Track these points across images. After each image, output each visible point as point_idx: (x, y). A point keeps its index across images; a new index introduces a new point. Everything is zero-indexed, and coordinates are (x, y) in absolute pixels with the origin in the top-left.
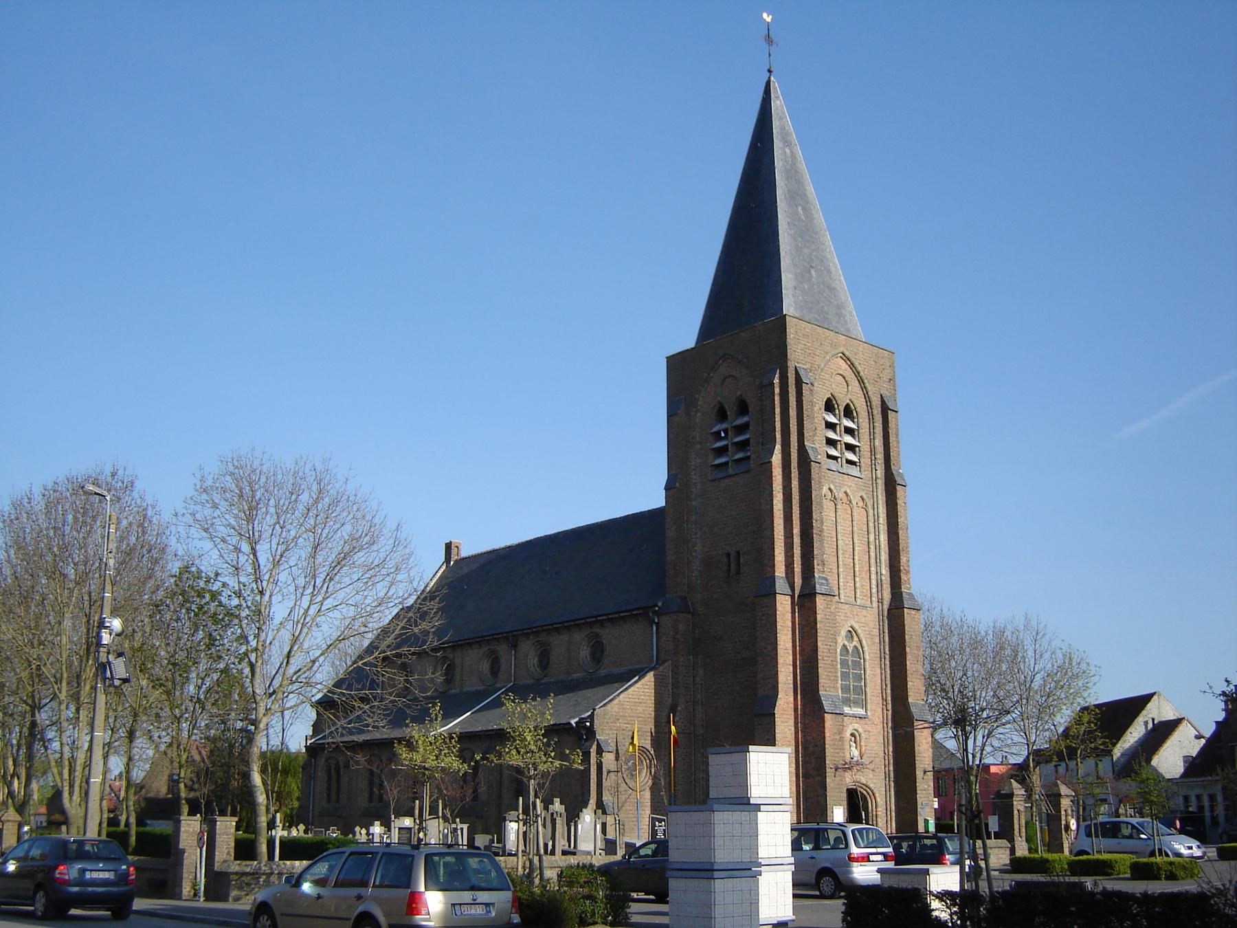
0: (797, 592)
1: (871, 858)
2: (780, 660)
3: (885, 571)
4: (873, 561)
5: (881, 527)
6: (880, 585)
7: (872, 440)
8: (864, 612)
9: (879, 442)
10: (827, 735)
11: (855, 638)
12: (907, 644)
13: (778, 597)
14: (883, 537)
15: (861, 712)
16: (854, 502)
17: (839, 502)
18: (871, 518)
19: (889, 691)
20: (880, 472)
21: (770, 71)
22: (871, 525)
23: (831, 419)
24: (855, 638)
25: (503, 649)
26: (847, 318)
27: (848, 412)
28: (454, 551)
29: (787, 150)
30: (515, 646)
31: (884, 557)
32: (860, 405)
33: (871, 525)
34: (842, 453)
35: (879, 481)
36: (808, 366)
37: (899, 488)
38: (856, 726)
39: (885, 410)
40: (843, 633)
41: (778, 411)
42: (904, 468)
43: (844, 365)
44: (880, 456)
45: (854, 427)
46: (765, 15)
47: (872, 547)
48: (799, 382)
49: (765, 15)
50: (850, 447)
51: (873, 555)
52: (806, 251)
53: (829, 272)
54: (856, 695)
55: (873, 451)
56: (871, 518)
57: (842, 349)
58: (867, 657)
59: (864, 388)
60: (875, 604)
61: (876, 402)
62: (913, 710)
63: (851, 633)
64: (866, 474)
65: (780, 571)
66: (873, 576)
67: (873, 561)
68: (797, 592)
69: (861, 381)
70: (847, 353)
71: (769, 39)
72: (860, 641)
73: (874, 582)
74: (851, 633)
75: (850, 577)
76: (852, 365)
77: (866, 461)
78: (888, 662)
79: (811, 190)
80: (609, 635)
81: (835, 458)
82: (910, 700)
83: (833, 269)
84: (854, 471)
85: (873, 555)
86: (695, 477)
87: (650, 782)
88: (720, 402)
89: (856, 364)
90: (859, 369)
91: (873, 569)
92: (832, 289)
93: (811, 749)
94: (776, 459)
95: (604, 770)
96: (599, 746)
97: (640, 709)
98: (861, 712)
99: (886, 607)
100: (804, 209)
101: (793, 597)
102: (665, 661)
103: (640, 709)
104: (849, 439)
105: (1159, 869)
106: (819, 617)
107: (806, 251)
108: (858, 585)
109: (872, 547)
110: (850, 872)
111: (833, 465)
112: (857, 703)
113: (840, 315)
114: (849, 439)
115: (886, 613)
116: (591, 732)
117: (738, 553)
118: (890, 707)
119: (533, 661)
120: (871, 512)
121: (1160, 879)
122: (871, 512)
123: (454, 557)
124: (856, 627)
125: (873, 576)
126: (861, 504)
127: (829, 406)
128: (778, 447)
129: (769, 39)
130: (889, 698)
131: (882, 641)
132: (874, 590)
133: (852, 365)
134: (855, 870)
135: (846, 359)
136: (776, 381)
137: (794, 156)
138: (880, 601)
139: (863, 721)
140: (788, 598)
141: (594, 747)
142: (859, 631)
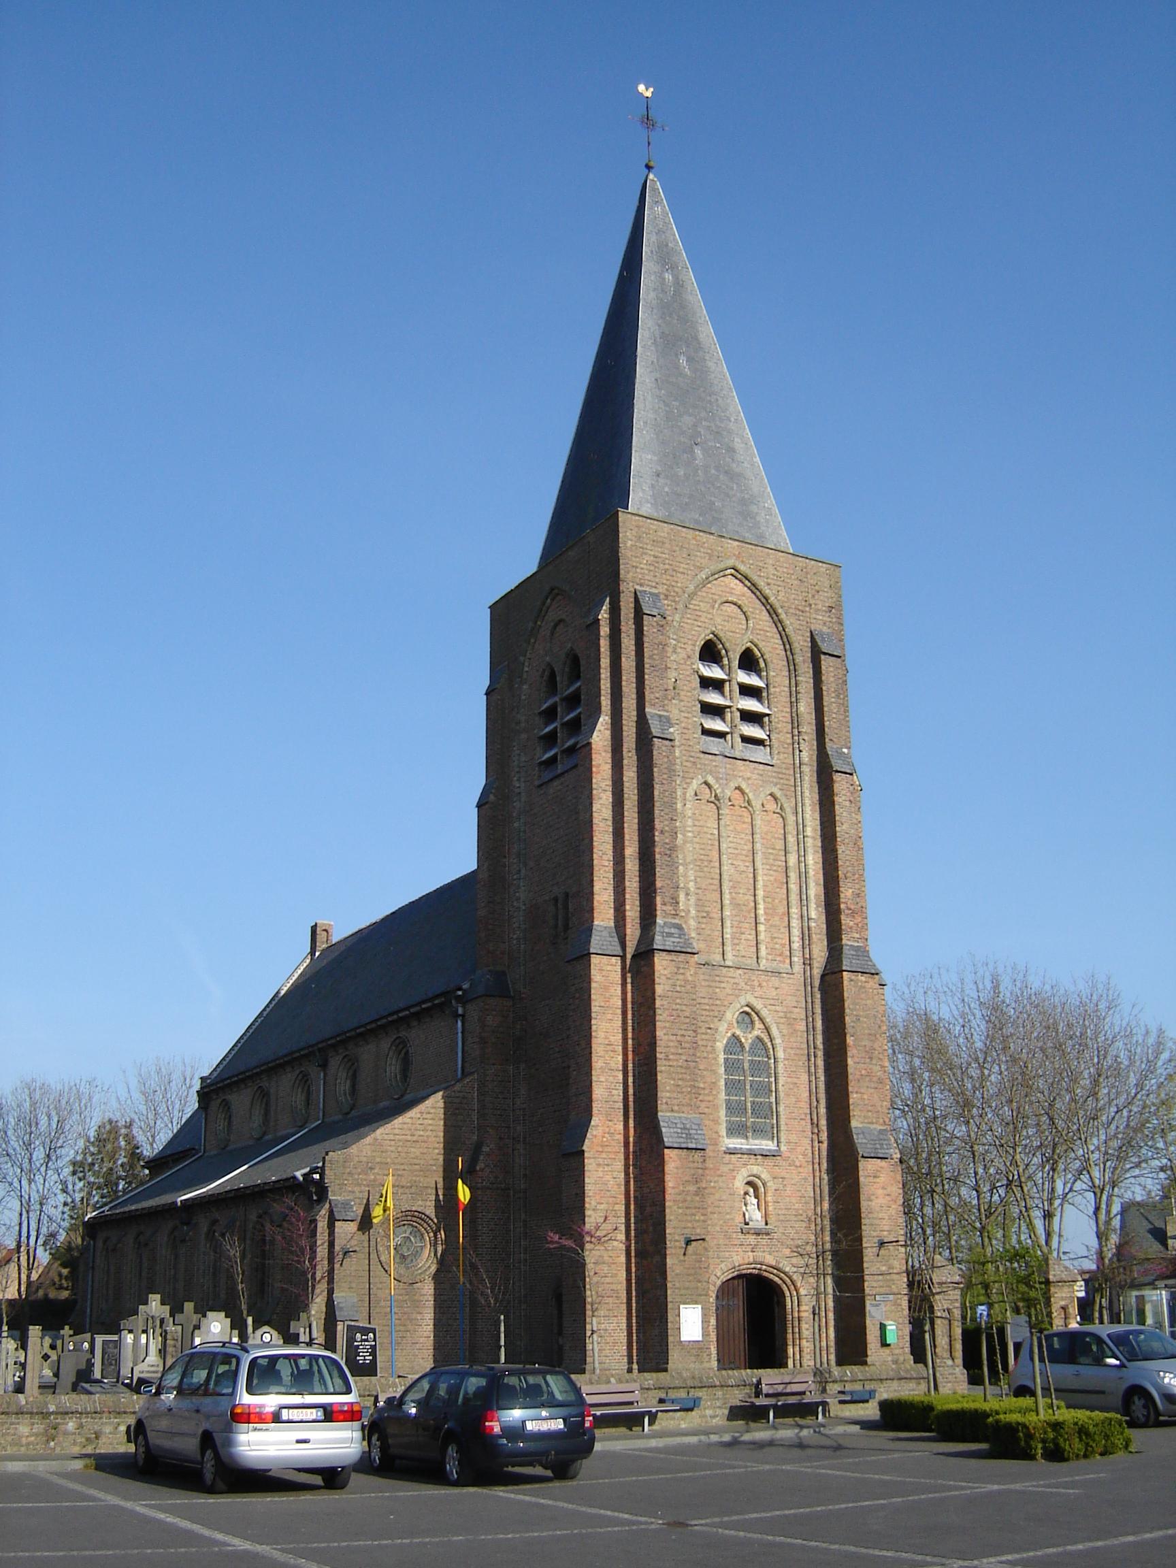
0: (629, 956)
1: (285, 1414)
2: (597, 1063)
3: (816, 913)
4: (794, 898)
5: (809, 842)
6: (806, 936)
7: (794, 703)
8: (775, 981)
9: (806, 707)
10: (670, 1183)
11: (758, 1025)
12: (849, 1030)
13: (595, 960)
14: (814, 860)
15: (768, 1145)
16: (757, 804)
17: (725, 804)
18: (791, 828)
19: (823, 1110)
20: (808, 754)
21: (649, 167)
22: (791, 839)
23: (715, 672)
24: (758, 1025)
25: (313, 1071)
26: (761, 518)
27: (749, 661)
28: (321, 936)
29: (668, 277)
30: (324, 1066)
31: (815, 890)
32: (770, 648)
33: (791, 839)
34: (734, 726)
35: (806, 769)
36: (661, 589)
37: (837, 777)
38: (756, 1169)
39: (816, 654)
40: (731, 1015)
41: (605, 662)
42: (858, 746)
43: (738, 589)
44: (808, 728)
45: (761, 684)
46: (641, 88)
47: (793, 876)
48: (639, 614)
49: (641, 88)
50: (749, 717)
51: (794, 887)
52: (687, 420)
53: (731, 450)
54: (753, 1114)
55: (795, 721)
56: (791, 828)
57: (731, 563)
58: (780, 1054)
59: (778, 622)
60: (798, 968)
61: (801, 644)
62: (858, 1140)
63: (749, 1016)
64: (781, 758)
65: (603, 917)
66: (795, 923)
67: (794, 898)
68: (630, 951)
69: (772, 612)
70: (742, 568)
71: (648, 121)
72: (767, 1029)
73: (796, 932)
74: (749, 1016)
75: (748, 926)
76: (754, 588)
77: (782, 737)
78: (820, 1063)
79: (707, 332)
80: (416, 1036)
81: (721, 735)
82: (854, 1123)
83: (738, 444)
84: (760, 754)
85: (794, 887)
86: (518, 784)
87: (434, 1268)
88: (549, 664)
89: (761, 584)
90: (767, 591)
91: (794, 911)
92: (733, 476)
93: (648, 1209)
94: (600, 737)
95: (337, 1248)
96: (331, 1212)
97: (415, 1151)
98: (768, 1145)
99: (817, 972)
100: (690, 360)
101: (623, 958)
102: (472, 1073)
103: (415, 1151)
104: (751, 705)
105: (1030, 1436)
106: (659, 990)
107: (687, 420)
108: (762, 937)
109: (793, 876)
110: (229, 1443)
111: (714, 744)
112: (758, 1132)
113: (746, 515)
114: (751, 705)
115: (817, 983)
116: (322, 1190)
117: (567, 895)
118: (824, 1136)
119: (344, 1086)
120: (791, 819)
121: (1032, 1458)
122: (791, 819)
123: (321, 946)
124: (758, 1005)
125: (795, 923)
126: (771, 806)
127: (710, 652)
128: (604, 720)
129: (648, 121)
130: (823, 1122)
131: (811, 1028)
132: (796, 945)
133: (754, 588)
134: (242, 1438)
135: (744, 578)
136: (604, 615)
137: (679, 285)
138: (808, 962)
139: (769, 1162)
140: (617, 961)
141: (324, 1212)
142: (764, 1013)
